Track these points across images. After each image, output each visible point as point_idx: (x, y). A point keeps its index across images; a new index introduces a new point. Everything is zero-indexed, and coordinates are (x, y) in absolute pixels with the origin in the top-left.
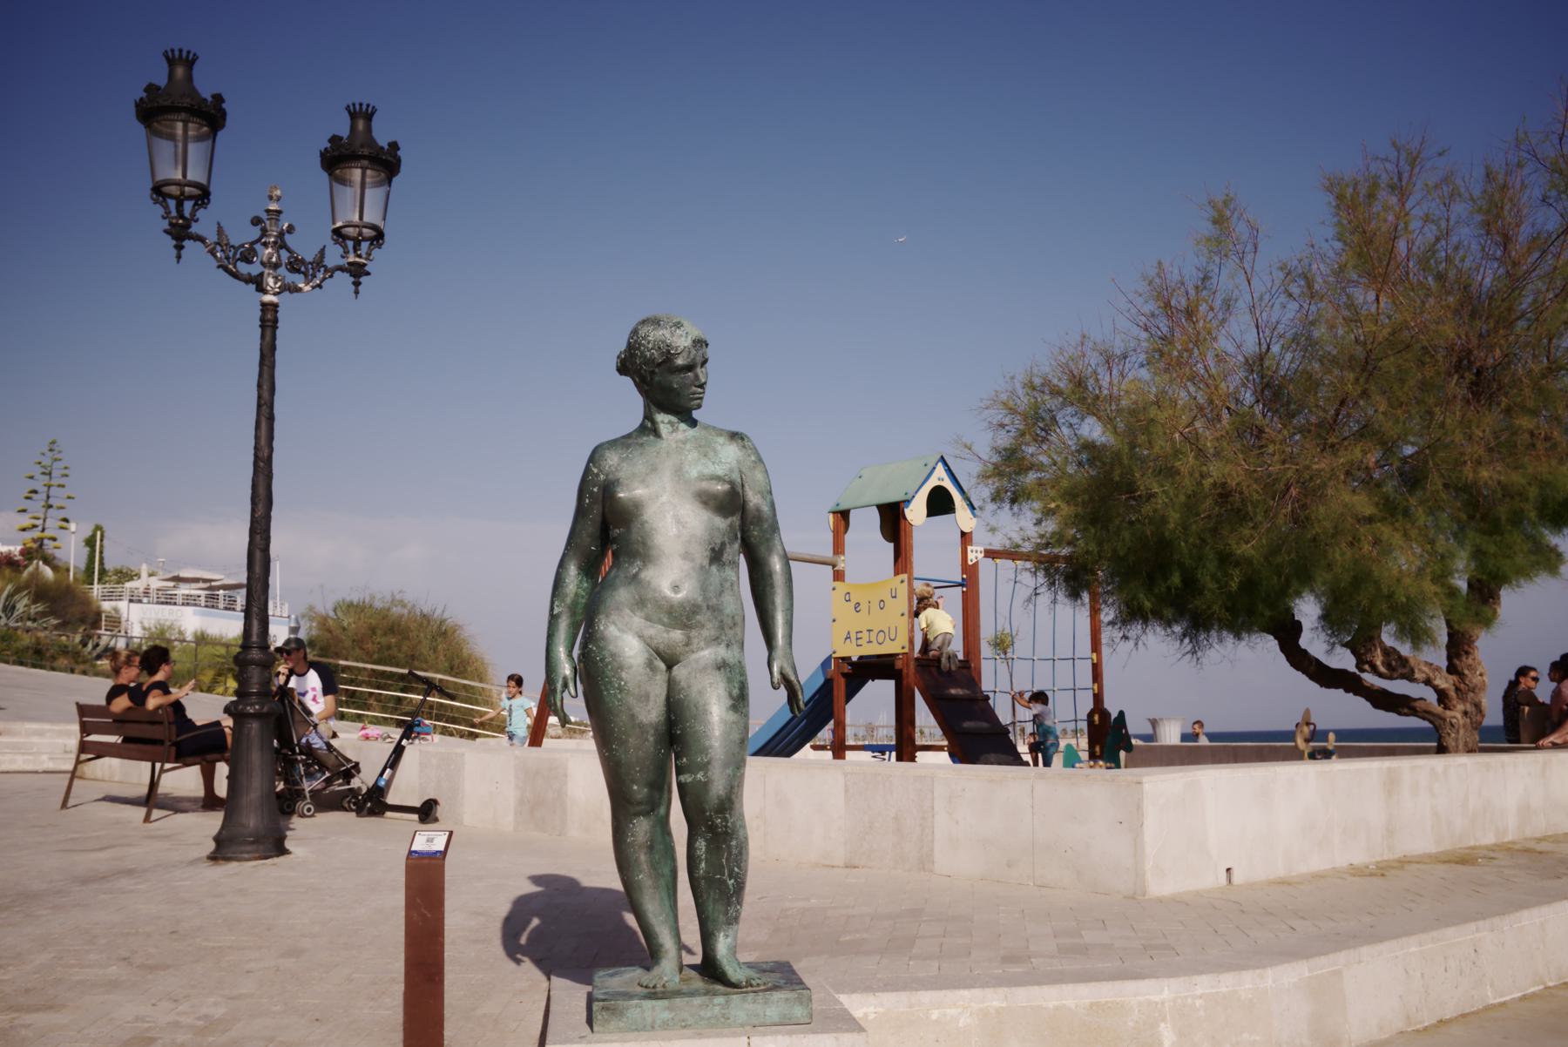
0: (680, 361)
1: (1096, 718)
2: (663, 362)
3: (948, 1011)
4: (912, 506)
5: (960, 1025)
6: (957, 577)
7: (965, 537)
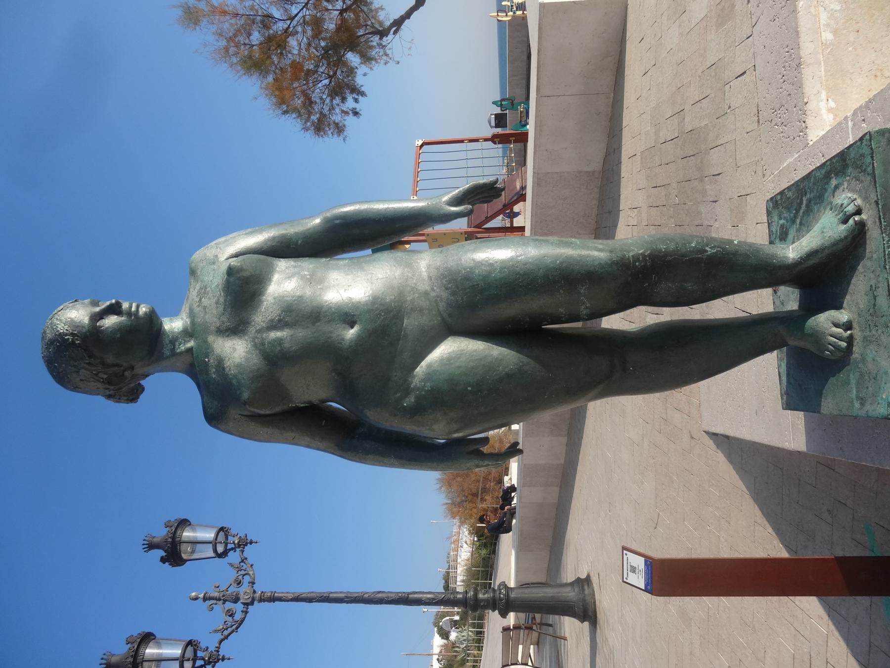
3: (823, 22)
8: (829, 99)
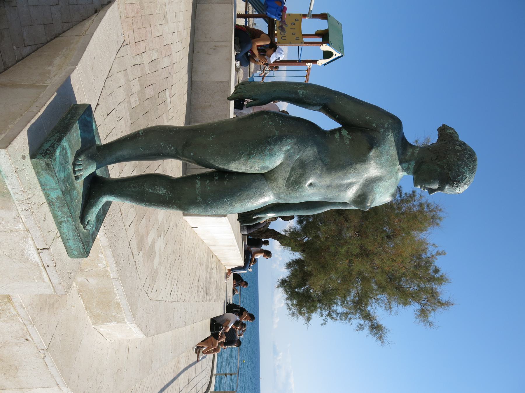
7: (315, 62)
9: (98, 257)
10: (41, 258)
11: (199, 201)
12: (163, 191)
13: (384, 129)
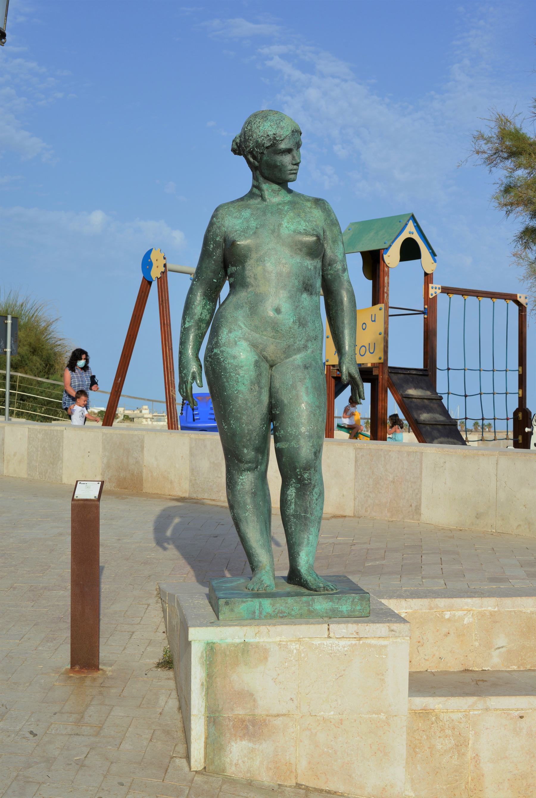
0: (283, 146)
1: (520, 415)
2: (272, 146)
4: (390, 252)
5: (465, 622)
6: (421, 306)
7: (428, 277)
8: (407, 614)
9: (449, 620)
10: (343, 637)
11: (295, 444)
12: (292, 490)
13: (222, 226)
